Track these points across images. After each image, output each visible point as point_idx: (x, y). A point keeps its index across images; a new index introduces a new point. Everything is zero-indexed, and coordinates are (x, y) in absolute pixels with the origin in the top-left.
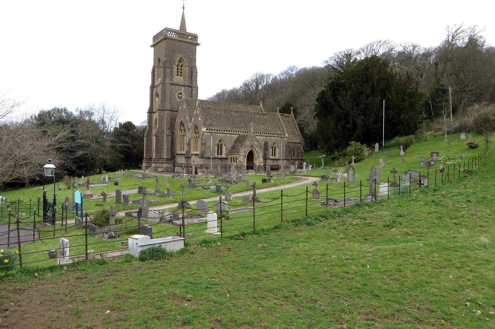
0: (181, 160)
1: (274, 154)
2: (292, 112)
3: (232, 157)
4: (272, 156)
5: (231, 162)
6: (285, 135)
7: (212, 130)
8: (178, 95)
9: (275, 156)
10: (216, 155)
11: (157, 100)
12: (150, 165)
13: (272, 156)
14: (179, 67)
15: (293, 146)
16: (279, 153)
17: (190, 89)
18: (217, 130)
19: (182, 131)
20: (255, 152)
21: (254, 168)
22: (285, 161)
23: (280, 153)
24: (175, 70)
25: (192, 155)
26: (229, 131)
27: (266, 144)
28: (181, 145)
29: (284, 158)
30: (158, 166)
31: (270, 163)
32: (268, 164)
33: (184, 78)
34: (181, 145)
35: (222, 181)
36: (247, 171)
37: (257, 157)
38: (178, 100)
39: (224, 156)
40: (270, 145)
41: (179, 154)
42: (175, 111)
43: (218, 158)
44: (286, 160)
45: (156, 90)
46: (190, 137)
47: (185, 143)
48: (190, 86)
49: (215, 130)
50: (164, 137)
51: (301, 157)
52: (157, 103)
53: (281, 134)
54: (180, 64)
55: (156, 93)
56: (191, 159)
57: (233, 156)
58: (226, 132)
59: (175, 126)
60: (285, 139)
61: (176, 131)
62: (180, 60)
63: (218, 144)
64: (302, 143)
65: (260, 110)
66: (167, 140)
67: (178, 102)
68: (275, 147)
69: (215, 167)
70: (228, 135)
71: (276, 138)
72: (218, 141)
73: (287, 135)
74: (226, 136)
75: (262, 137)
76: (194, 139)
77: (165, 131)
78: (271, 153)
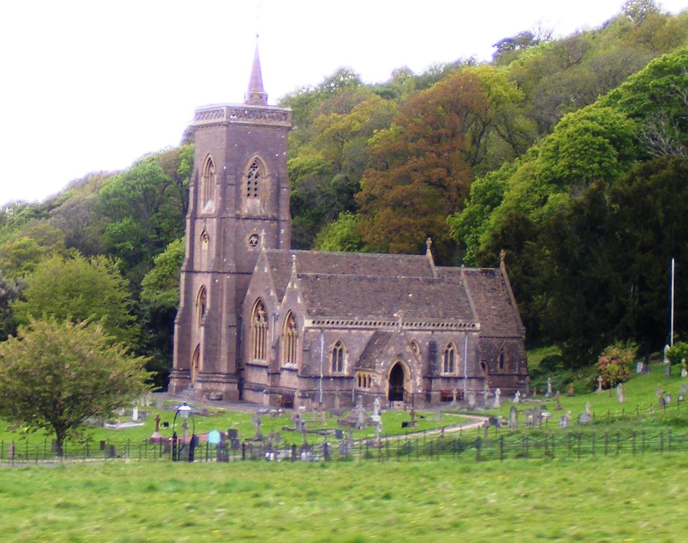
0: (259, 378)
1: (450, 366)
2: (502, 263)
3: (362, 376)
4: (446, 371)
5: (360, 385)
6: (473, 326)
7: (323, 322)
8: (250, 238)
9: (451, 371)
10: (330, 371)
11: (205, 245)
12: (185, 385)
13: (446, 371)
14: (253, 177)
15: (500, 344)
16: (461, 366)
17: (275, 224)
18: (333, 323)
19: (259, 317)
20: (407, 367)
21: (404, 397)
22: (473, 381)
23: (461, 364)
24: (244, 186)
25: (283, 369)
26: (357, 323)
27: (433, 347)
28: (258, 347)
29: (472, 374)
30: (209, 388)
31: (438, 386)
32: (437, 389)
33: (263, 201)
34: (258, 347)
35: (343, 423)
36: (390, 404)
37: (411, 376)
38: (250, 249)
39: (345, 372)
40: (441, 347)
41: (253, 366)
42: (244, 273)
43: (334, 378)
44: (475, 378)
45: (204, 224)
46: (278, 333)
47: (268, 342)
48: (273, 217)
49: (328, 323)
50: (221, 328)
51: (519, 370)
52: (205, 255)
53: (465, 325)
54: (255, 173)
55: (203, 233)
56: (280, 378)
57: (363, 373)
58: (350, 326)
59: (244, 306)
60: (475, 334)
61: (245, 316)
62: (254, 164)
63: (335, 350)
64: (521, 338)
65: (426, 264)
66: (229, 335)
67: (249, 253)
68: (452, 351)
69: (330, 395)
70: (353, 332)
71: (455, 333)
72: (334, 344)
73: (478, 326)
74: (350, 333)
75: (424, 333)
76: (287, 338)
77: (224, 315)
78: (443, 366)
